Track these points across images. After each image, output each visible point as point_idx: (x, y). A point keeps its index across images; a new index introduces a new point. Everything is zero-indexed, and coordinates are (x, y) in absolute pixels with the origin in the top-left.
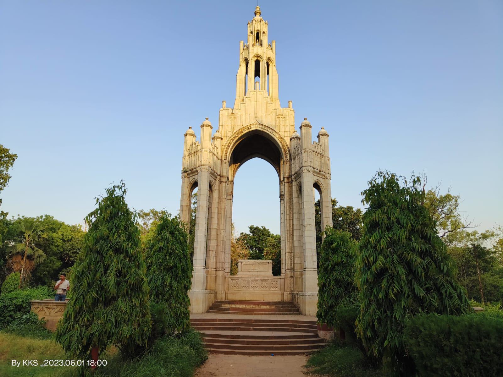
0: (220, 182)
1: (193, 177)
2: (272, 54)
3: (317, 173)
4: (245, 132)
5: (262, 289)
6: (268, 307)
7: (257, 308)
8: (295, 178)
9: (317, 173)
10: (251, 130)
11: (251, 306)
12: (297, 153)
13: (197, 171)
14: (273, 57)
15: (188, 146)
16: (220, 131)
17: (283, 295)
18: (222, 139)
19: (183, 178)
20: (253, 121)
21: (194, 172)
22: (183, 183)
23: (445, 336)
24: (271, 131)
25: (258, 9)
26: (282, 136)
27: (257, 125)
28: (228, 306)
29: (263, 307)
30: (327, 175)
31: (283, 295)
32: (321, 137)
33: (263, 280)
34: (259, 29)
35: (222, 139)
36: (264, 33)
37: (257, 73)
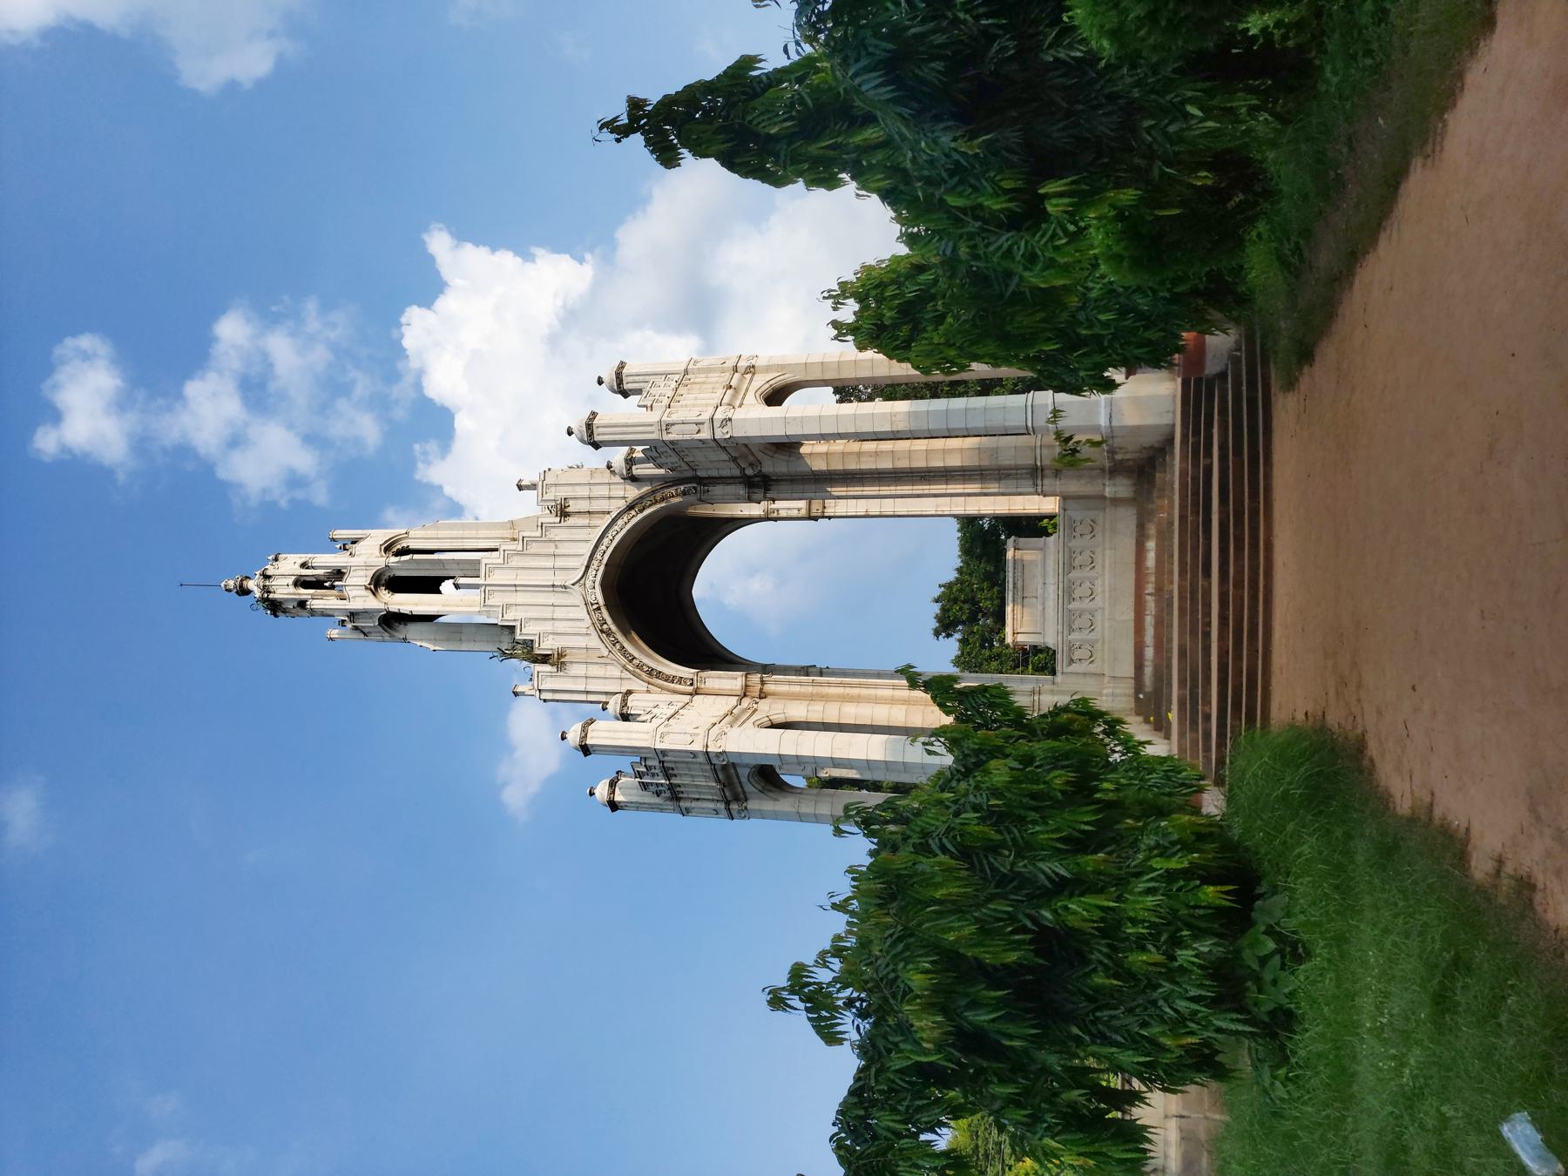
0: (763, 695)
1: (744, 780)
2: (376, 538)
3: (734, 396)
4: (609, 620)
5: (1098, 568)
6: (1151, 545)
7: (1153, 579)
8: (751, 465)
9: (734, 396)
10: (601, 602)
11: (1149, 598)
12: (675, 459)
13: (724, 768)
14: (379, 536)
15: (649, 798)
16: (603, 698)
17: (1116, 502)
18: (629, 692)
19: (745, 814)
20: (575, 597)
21: (728, 777)
22: (762, 815)
23: (1130, 1011)
24: (606, 541)
25: (231, 583)
26: (622, 504)
27: (589, 584)
28: (1148, 670)
29: (1151, 559)
30: (743, 364)
31: (1116, 502)
32: (597, 438)
33: (1069, 566)
34: (291, 580)
35: (629, 692)
36: (304, 565)
37: (430, 585)
